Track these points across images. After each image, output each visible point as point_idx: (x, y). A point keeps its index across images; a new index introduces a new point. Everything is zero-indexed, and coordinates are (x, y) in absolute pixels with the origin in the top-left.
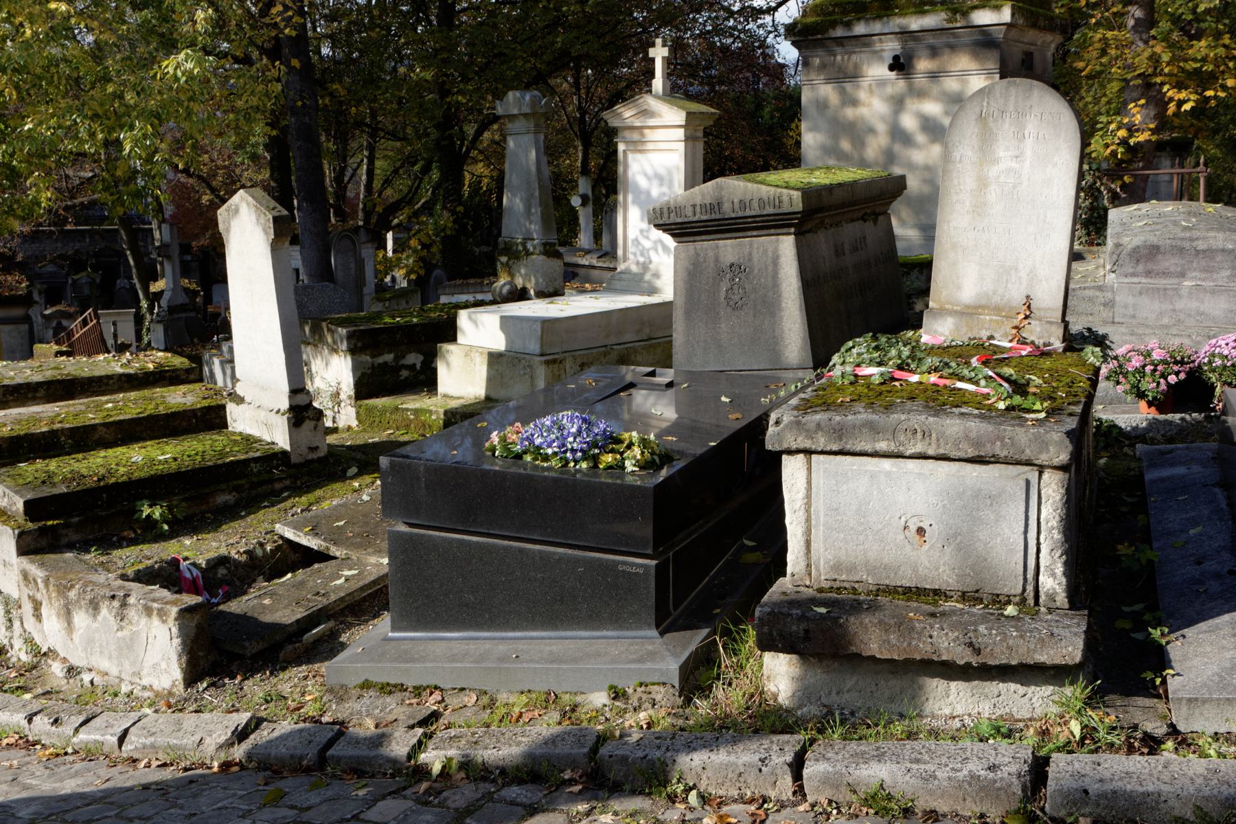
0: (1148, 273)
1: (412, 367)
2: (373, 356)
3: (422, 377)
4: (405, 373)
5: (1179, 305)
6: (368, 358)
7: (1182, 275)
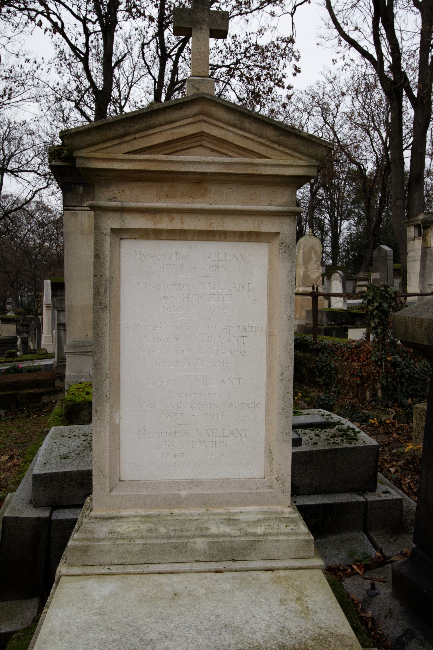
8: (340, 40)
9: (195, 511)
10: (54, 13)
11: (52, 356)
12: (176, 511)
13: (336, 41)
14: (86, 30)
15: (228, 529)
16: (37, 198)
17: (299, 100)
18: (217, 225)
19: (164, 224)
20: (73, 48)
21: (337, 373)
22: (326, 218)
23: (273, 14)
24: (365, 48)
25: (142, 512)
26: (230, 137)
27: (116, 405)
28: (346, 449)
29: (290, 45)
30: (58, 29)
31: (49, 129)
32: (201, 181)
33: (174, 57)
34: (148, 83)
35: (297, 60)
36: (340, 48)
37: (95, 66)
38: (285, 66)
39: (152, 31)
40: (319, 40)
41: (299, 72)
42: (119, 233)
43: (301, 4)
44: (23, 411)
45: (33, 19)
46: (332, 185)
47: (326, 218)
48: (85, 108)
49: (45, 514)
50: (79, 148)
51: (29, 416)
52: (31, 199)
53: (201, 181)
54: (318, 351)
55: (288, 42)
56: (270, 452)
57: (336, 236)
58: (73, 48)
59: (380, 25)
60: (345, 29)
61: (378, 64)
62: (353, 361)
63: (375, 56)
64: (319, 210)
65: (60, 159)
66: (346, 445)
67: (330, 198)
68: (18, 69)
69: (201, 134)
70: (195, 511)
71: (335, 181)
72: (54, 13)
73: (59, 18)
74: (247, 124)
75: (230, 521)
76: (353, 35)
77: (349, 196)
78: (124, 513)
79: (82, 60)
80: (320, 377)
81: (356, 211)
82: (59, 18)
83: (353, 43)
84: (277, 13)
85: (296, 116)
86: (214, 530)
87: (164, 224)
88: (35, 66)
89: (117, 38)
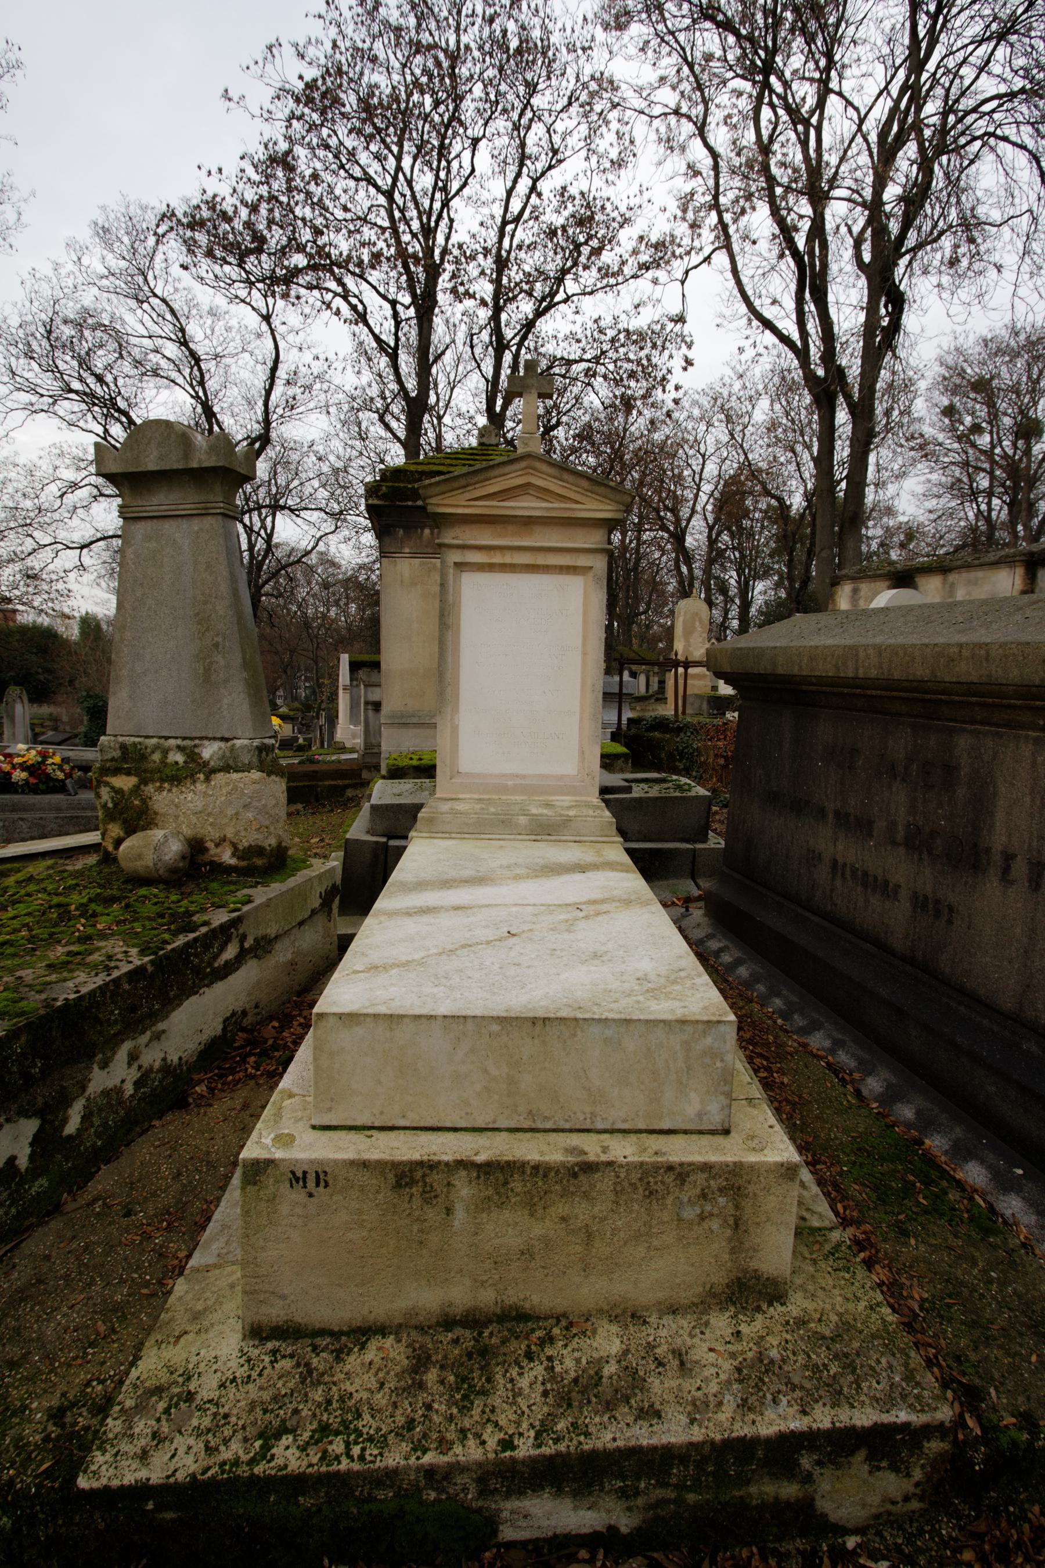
8: (750, 320)
9: (519, 798)
10: (355, 296)
11: (352, 750)
12: (504, 797)
13: (745, 320)
14: (395, 315)
15: (545, 811)
16: (321, 547)
17: (695, 403)
18: (541, 559)
19: (497, 559)
20: (377, 339)
21: (700, 754)
22: (732, 577)
23: (655, 281)
24: (785, 332)
25: (476, 796)
26: (552, 487)
27: (456, 709)
28: (676, 798)
29: (679, 325)
30: (362, 317)
31: (341, 449)
32: (528, 523)
33: (514, 349)
34: (476, 382)
35: (689, 347)
36: (748, 332)
37: (407, 362)
38: (671, 356)
39: (484, 314)
40: (719, 321)
41: (692, 365)
42: (460, 566)
43: (696, 267)
44: (324, 806)
45: (328, 306)
46: (740, 528)
47: (732, 577)
48: (394, 424)
49: (384, 840)
50: (431, 497)
51: (332, 811)
52: (313, 548)
53: (528, 523)
54: (679, 730)
55: (676, 322)
56: (582, 753)
57: (746, 605)
58: (377, 339)
59: (807, 296)
60: (757, 303)
61: (802, 354)
62: (719, 740)
63: (799, 343)
64: (722, 565)
65: (378, 497)
66: (677, 794)
67: (739, 548)
68: (303, 370)
69: (529, 484)
70: (519, 798)
71: (747, 523)
72: (355, 296)
73: (361, 302)
74: (565, 476)
75: (548, 805)
76: (768, 313)
77: (766, 545)
78: (461, 796)
79: (388, 354)
80: (680, 761)
81: (776, 566)
82: (361, 302)
83: (768, 325)
84: (661, 280)
85: (690, 427)
86: (534, 811)
87: (497, 559)
88: (326, 364)
89: (438, 321)
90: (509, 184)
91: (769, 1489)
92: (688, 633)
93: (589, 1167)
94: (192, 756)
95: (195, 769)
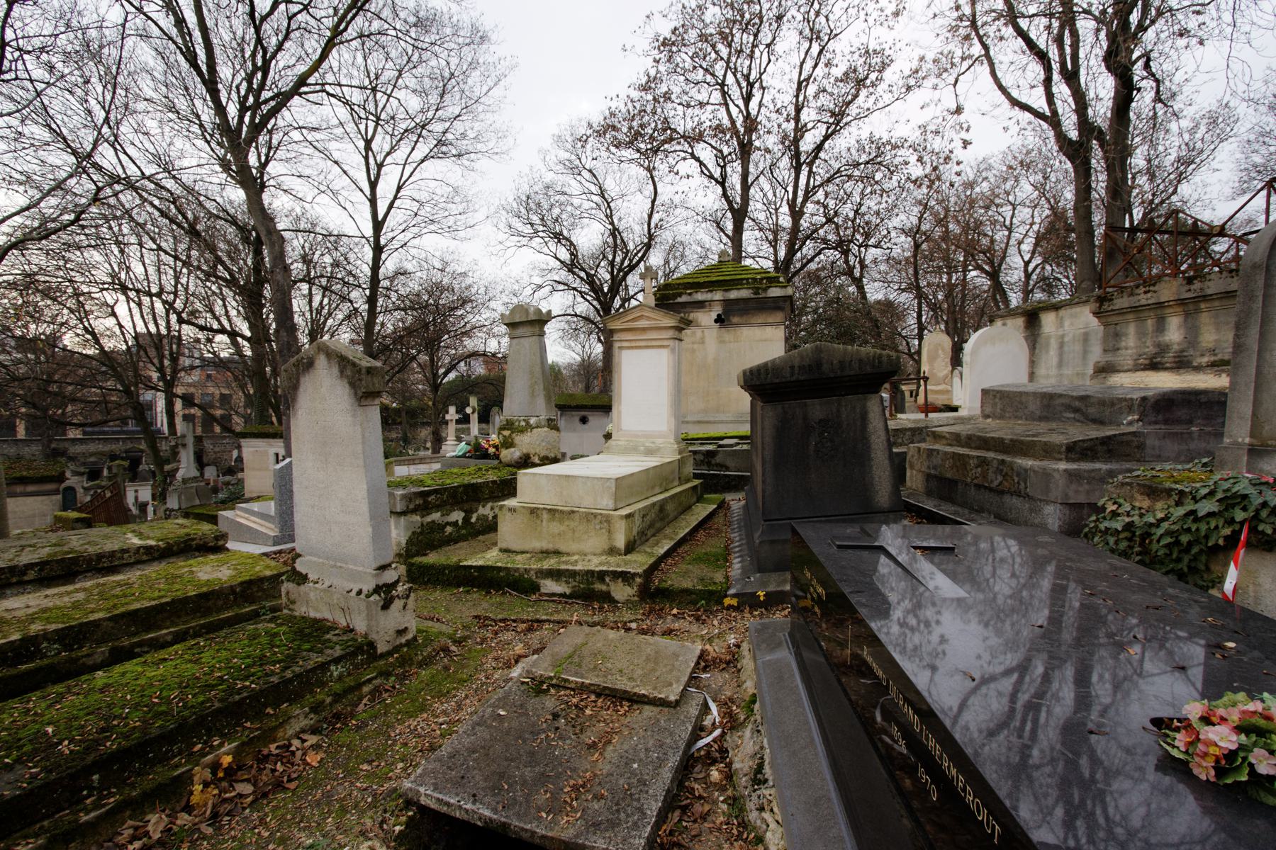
0: (1166, 422)
1: (455, 524)
2: (422, 517)
3: (464, 532)
4: (449, 529)
5: (1192, 446)
6: (418, 518)
7: (1190, 422)
18: (650, 343)
19: (633, 344)
32: (644, 330)
53: (644, 330)
83: (1025, 107)
87: (633, 344)
90: (802, 57)
91: (599, 587)
92: (932, 359)
93: (573, 512)
94: (528, 423)
95: (529, 427)
